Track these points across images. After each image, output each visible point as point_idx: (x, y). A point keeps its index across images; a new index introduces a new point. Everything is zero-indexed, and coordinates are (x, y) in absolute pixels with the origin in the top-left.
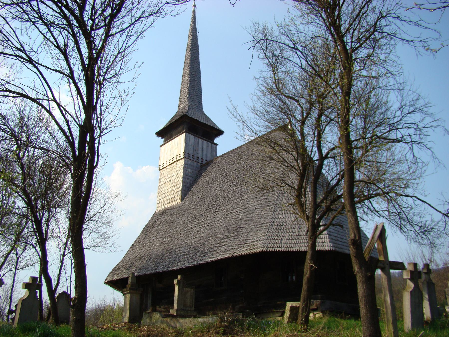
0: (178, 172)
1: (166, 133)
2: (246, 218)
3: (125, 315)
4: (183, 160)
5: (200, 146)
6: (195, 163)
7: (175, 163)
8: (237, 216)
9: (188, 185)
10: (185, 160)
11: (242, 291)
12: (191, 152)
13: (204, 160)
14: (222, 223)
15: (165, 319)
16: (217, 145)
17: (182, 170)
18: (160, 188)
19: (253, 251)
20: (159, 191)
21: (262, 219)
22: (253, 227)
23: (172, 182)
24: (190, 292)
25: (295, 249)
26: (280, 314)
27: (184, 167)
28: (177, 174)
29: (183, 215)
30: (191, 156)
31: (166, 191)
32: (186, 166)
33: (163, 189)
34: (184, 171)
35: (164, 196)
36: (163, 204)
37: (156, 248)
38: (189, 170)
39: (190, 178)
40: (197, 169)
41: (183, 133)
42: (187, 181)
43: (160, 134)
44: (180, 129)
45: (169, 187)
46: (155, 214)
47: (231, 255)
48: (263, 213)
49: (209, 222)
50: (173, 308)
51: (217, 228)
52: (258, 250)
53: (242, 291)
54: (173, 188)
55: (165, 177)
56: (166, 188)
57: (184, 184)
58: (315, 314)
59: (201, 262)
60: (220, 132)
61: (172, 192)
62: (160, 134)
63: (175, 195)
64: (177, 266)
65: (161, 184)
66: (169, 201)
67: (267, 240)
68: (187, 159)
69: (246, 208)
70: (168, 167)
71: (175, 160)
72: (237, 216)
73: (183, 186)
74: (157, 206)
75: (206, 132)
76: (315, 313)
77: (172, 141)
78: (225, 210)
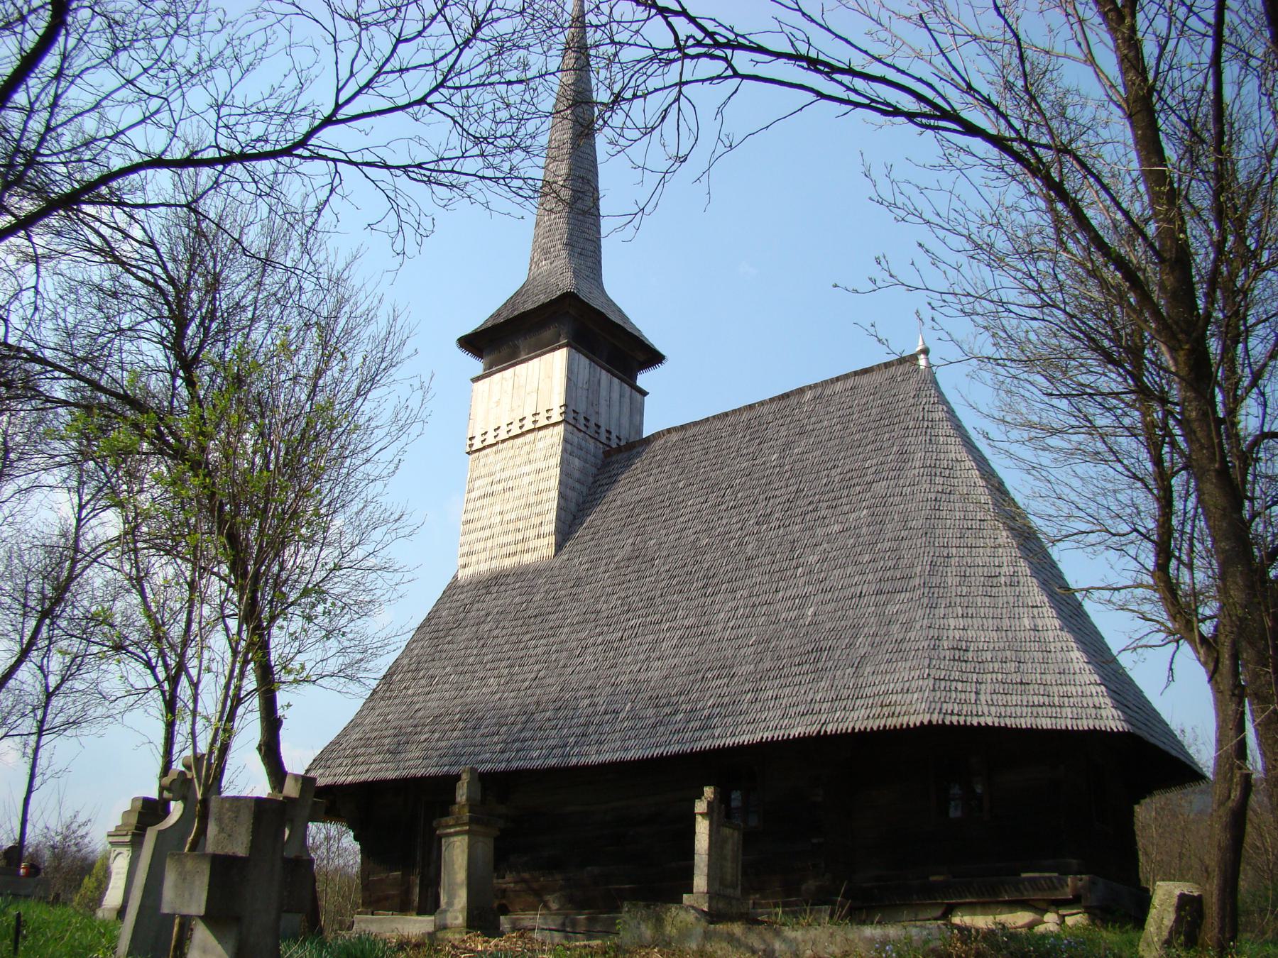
0: (542, 465)
1: (497, 342)
2: (831, 620)
3: (450, 904)
4: (561, 428)
5: (604, 393)
6: (592, 441)
7: (530, 437)
8: (793, 614)
9: (573, 506)
10: (565, 430)
11: (815, 841)
12: (582, 408)
13: (613, 437)
14: (741, 632)
15: (720, 927)
16: (644, 393)
17: (557, 460)
18: (470, 506)
19: (891, 722)
20: (469, 517)
21: (895, 628)
22: (867, 648)
23: (517, 493)
24: (732, 836)
25: (1024, 723)
26: (938, 912)
27: (564, 450)
28: (539, 471)
29: (574, 597)
30: (582, 421)
31: (497, 519)
32: (569, 447)
33: (485, 512)
34: (564, 464)
35: (488, 532)
36: (483, 556)
37: (490, 689)
38: (576, 461)
39: (577, 486)
40: (601, 458)
41: (560, 347)
42: (570, 493)
43: (474, 343)
44: (548, 334)
45: (509, 506)
46: (454, 588)
47: (813, 730)
48: (892, 609)
49: (687, 623)
50: (690, 891)
51: (724, 644)
52: (915, 720)
53: (815, 841)
54: (526, 512)
55: (490, 475)
56: (497, 509)
57: (562, 501)
58: (1064, 916)
59: (697, 746)
60: (653, 358)
61: (521, 524)
62: (474, 343)
63: (531, 533)
64: (599, 752)
65: (473, 495)
66: (505, 551)
67: (934, 690)
68: (570, 428)
69: (824, 591)
70: (500, 446)
71: (528, 425)
72: (793, 614)
73: (560, 508)
74: (461, 561)
75: (615, 350)
76: (1062, 912)
77: (518, 367)
78: (745, 593)
